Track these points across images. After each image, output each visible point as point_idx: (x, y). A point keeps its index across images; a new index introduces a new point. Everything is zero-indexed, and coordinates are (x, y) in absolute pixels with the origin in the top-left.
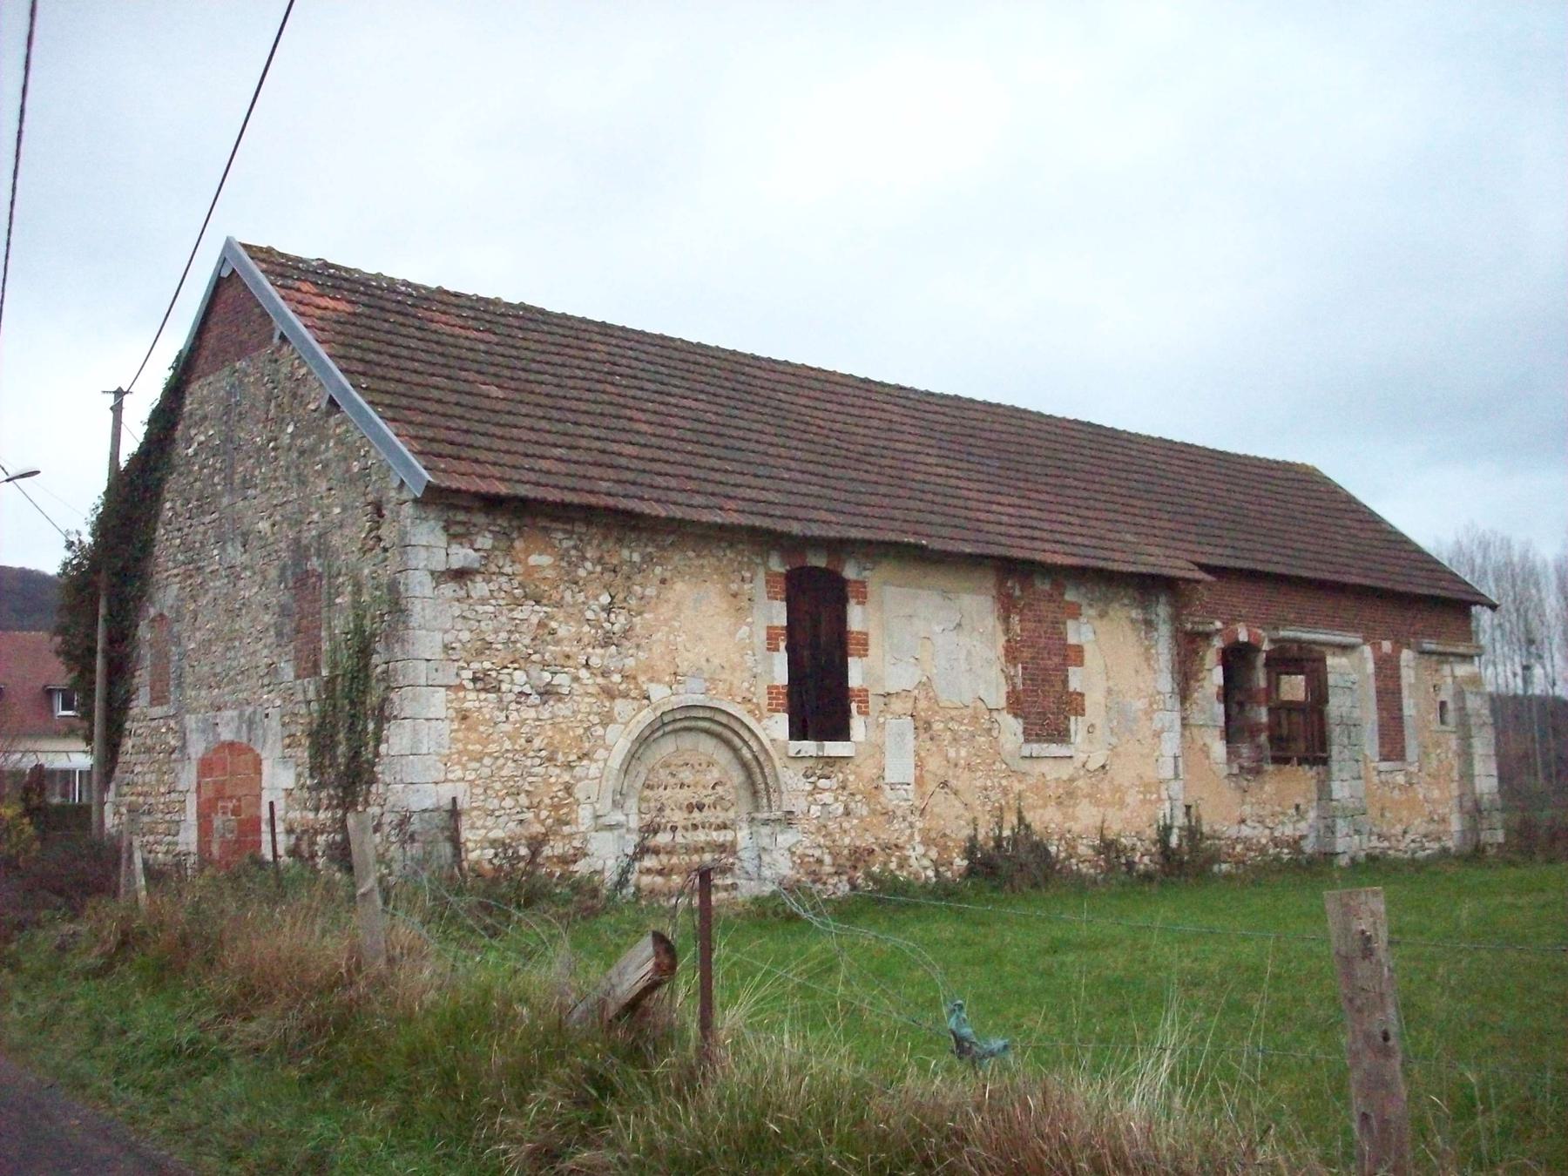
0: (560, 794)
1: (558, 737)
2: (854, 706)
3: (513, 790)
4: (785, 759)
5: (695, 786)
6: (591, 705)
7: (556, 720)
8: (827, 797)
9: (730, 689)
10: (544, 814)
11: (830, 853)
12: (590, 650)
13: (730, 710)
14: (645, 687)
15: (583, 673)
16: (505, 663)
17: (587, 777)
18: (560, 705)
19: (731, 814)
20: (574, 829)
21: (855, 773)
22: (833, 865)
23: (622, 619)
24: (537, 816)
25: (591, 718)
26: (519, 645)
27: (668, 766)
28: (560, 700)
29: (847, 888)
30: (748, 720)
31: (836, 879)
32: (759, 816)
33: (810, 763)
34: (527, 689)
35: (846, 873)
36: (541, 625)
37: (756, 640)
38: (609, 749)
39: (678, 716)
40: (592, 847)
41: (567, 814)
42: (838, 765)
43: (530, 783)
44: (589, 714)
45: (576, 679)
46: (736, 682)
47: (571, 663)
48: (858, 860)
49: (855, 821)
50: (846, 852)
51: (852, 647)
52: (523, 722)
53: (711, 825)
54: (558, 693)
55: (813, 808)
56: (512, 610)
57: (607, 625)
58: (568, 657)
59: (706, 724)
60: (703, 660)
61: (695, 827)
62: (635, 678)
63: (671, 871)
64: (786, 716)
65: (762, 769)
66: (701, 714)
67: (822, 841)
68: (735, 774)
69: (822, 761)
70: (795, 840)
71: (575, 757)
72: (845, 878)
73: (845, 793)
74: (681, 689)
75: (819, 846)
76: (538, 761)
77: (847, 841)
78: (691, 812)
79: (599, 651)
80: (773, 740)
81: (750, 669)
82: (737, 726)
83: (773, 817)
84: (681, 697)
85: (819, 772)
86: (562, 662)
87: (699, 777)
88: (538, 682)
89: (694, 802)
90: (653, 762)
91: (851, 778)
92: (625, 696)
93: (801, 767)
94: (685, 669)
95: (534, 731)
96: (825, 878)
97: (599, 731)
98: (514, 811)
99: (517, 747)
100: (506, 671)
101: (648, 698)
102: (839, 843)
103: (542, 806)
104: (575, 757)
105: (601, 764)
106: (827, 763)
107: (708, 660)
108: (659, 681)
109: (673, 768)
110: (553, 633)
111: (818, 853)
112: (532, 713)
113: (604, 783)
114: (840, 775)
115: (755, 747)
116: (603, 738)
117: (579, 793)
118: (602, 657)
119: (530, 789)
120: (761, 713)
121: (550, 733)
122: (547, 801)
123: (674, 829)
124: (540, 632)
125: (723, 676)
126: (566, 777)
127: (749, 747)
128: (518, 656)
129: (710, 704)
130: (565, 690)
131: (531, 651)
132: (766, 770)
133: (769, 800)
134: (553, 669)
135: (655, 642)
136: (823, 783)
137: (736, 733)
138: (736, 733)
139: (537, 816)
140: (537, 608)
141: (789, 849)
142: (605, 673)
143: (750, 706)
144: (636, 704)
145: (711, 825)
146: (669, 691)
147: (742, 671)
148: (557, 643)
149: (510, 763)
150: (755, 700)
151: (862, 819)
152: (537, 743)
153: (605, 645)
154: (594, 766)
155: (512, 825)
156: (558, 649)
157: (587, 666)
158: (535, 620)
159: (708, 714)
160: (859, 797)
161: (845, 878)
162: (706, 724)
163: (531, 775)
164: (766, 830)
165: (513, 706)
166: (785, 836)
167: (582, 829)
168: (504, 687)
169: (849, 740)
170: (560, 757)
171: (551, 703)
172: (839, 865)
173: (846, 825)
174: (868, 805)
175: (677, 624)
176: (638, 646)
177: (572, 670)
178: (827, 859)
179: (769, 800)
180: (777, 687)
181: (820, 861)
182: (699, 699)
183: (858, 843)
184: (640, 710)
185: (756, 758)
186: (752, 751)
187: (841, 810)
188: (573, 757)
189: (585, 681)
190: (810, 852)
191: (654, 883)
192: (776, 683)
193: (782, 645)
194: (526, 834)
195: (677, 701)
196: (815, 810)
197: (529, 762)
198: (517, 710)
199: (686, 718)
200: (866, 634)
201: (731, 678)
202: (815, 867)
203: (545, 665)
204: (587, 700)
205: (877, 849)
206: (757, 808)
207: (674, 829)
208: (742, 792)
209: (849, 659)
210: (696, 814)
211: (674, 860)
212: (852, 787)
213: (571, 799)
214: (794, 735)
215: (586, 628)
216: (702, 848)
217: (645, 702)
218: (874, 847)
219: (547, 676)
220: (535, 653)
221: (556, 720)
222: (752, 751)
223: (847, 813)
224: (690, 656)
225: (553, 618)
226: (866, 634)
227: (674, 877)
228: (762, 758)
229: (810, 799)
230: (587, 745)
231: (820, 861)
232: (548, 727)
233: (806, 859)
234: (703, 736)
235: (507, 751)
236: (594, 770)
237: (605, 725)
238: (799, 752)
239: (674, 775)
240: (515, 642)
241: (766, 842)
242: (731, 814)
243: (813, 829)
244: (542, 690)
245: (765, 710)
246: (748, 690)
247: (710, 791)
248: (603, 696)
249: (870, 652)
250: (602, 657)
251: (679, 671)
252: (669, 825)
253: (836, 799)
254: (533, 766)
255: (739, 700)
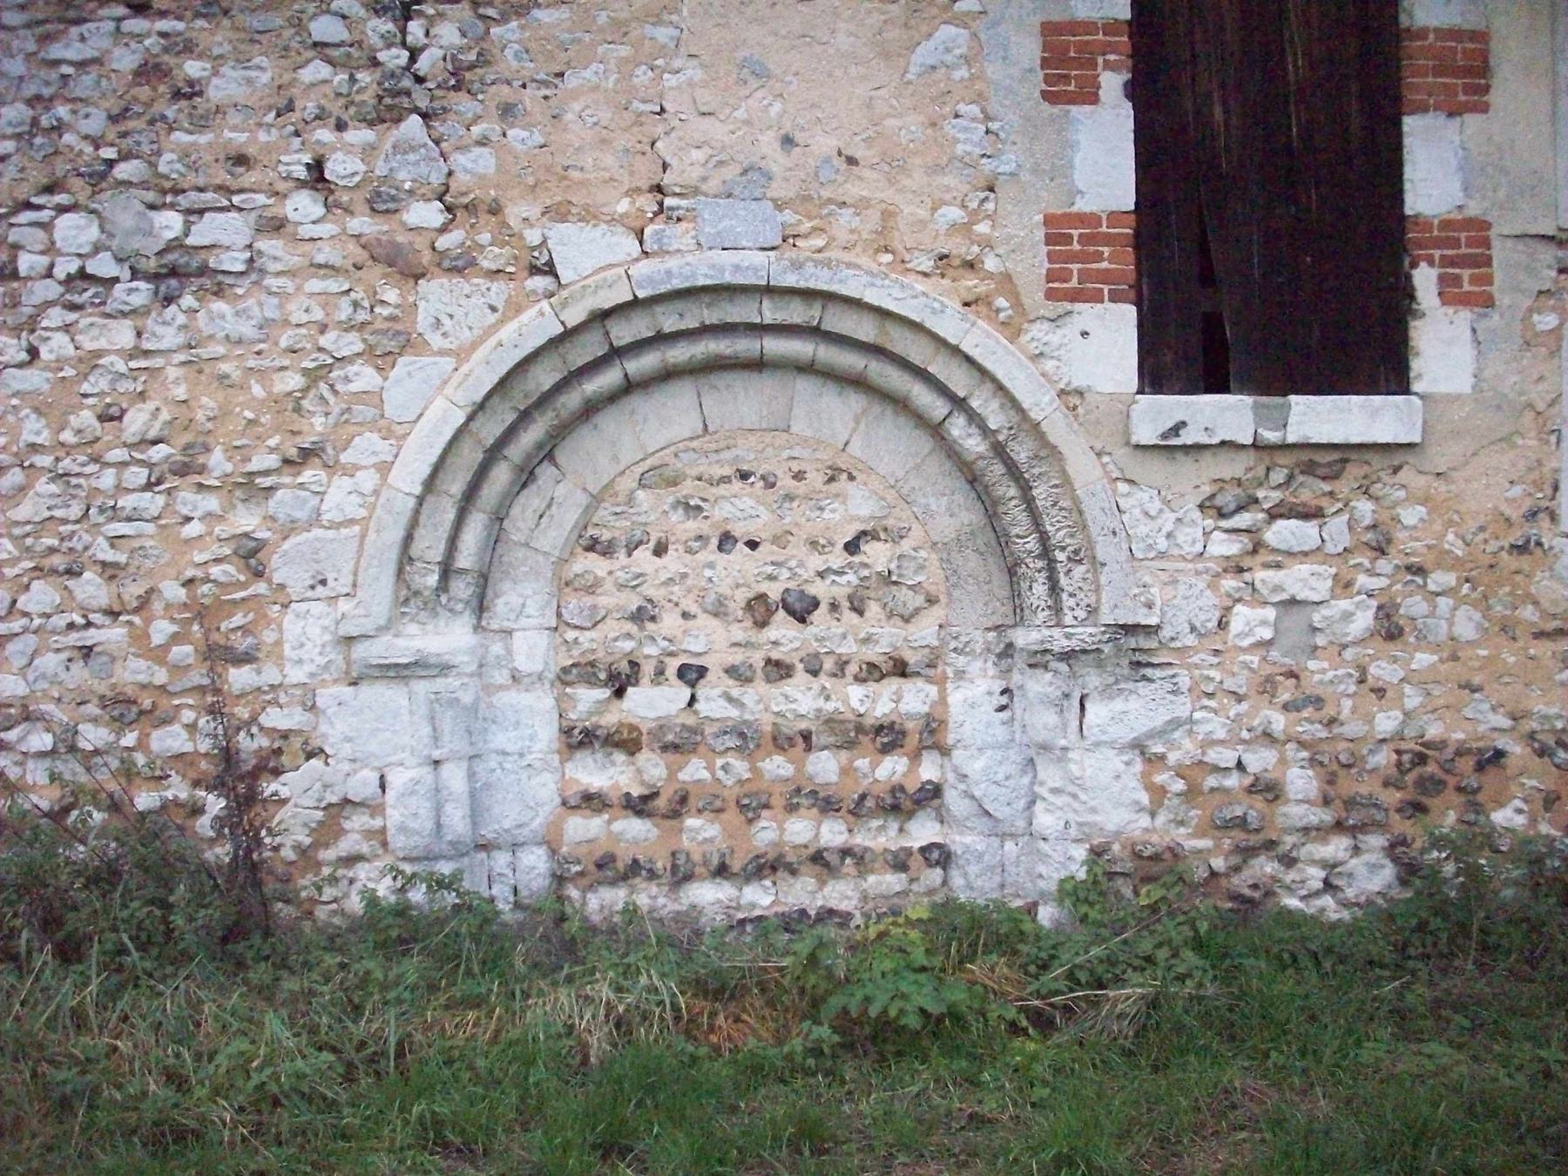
0: (216, 571)
1: (208, 402)
2: (1425, 279)
3: (58, 561)
4: (1121, 453)
5: (780, 540)
6: (326, 299)
7: (204, 352)
8: (1305, 580)
9: (883, 231)
10: (161, 630)
11: (1313, 762)
12: (325, 135)
13: (871, 297)
14: (533, 237)
15: (303, 206)
16: (22, 192)
17: (315, 520)
18: (219, 306)
19: (925, 631)
20: (270, 675)
21: (1425, 501)
22: (1326, 802)
23: (448, 34)
24: (139, 638)
25: (325, 341)
26: (68, 138)
27: (673, 482)
28: (219, 292)
29: (1388, 872)
30: (978, 338)
31: (1337, 847)
32: (1024, 638)
33: (1233, 467)
34: (103, 266)
35: (1381, 827)
36: (149, 71)
37: (993, 70)
38: (394, 433)
39: (670, 324)
40: (333, 731)
41: (244, 629)
42: (1354, 472)
43: (114, 541)
44: (323, 328)
45: (276, 226)
46: (911, 210)
47: (250, 178)
48: (1431, 786)
49: (1423, 659)
50: (1383, 758)
51: (1418, 80)
52: (90, 362)
53: (842, 664)
54: (204, 270)
55: (1242, 616)
56: (46, 39)
57: (395, 58)
58: (241, 160)
59: (800, 348)
60: (768, 143)
61: (779, 670)
62: (495, 210)
63: (681, 804)
64: (1129, 312)
65: (1026, 489)
66: (770, 313)
67: (1279, 722)
68: (937, 504)
69: (1284, 459)
70: (1160, 719)
71: (272, 461)
72: (1376, 841)
73: (1384, 565)
74: (679, 237)
75: (1268, 737)
76: (138, 475)
77: (1386, 723)
78: (762, 624)
79: (359, 135)
80: (1070, 396)
81: (967, 163)
82: (917, 351)
83: (1060, 643)
84: (673, 263)
85: (1269, 497)
86: (222, 177)
87: (795, 514)
88: (136, 243)
89: (774, 592)
90: (607, 470)
91: (1411, 515)
92: (460, 266)
93: (1195, 479)
94: (695, 174)
95: (126, 386)
96: (1289, 840)
97: (364, 377)
98: (60, 621)
99: (67, 436)
100: (26, 216)
101: (550, 269)
102: (1353, 728)
103: (157, 606)
104: (272, 461)
105: (367, 480)
106: (1310, 469)
107: (788, 141)
108: (590, 216)
109: (687, 488)
110: (190, 92)
111: (1260, 760)
112: (122, 334)
113: (372, 536)
114: (1364, 508)
115: (996, 418)
116: (375, 398)
117: (286, 568)
118: (368, 151)
119: (109, 556)
120: (1017, 303)
121: (181, 392)
122: (174, 592)
123: (692, 674)
124: (144, 92)
125: (853, 191)
126: (246, 520)
127: (974, 418)
128: (61, 167)
129: (791, 280)
130: (233, 261)
131: (109, 153)
132: (1040, 492)
133: (1054, 588)
134: (192, 199)
135: (575, 94)
136: (1284, 533)
137: (922, 374)
138: (922, 374)
139: (139, 638)
140: (136, 25)
141: (1139, 746)
142: (383, 201)
143: (970, 282)
144: (499, 291)
145: (842, 664)
146: (633, 247)
147: (937, 169)
148: (201, 123)
149: (44, 486)
150: (991, 264)
151: (1453, 651)
152: (136, 421)
153: (386, 113)
154: (341, 484)
155: (50, 662)
156: (203, 139)
157: (317, 177)
158: (125, 60)
159: (796, 313)
160: (1440, 579)
161: (1376, 841)
162: (800, 348)
163: (114, 513)
164: (1039, 685)
165: (56, 317)
166: (1118, 705)
167: (296, 675)
168: (25, 263)
169: (1403, 387)
170: (218, 462)
171: (188, 301)
172: (1350, 803)
173: (1383, 671)
174: (1483, 604)
175: (663, 34)
176: (507, 111)
177: (261, 199)
178: (1300, 781)
179: (1054, 588)
180: (1083, 219)
181: (1269, 790)
182: (752, 265)
183: (1434, 731)
184: (514, 308)
185: (999, 450)
186: (985, 431)
187: (1364, 620)
188: (262, 461)
189: (307, 231)
190: (1226, 757)
191: (616, 838)
192: (1082, 206)
193: (1112, 83)
194: (103, 688)
195: (651, 276)
196: (1251, 622)
197: (108, 479)
198: (67, 328)
199: (706, 330)
200: (1480, 36)
201: (889, 194)
202: (1253, 809)
203: (165, 193)
204: (315, 285)
205: (1516, 750)
206: (1020, 613)
207: (692, 674)
208: (970, 562)
209: (1409, 123)
210: (782, 629)
211: (695, 770)
212: (1410, 545)
213: (261, 588)
214: (1154, 377)
215: (317, 70)
216: (806, 736)
217: (540, 283)
218: (1501, 742)
219: (169, 223)
220: (125, 156)
221: (204, 352)
222: (985, 431)
223: (1390, 629)
224: (716, 130)
225: (188, 48)
226: (1480, 36)
227: (691, 822)
228: (1021, 452)
229: (1230, 583)
230: (319, 423)
231: (1269, 790)
232: (172, 373)
233: (1211, 781)
234: (804, 386)
235: (34, 448)
236: (340, 497)
237: (382, 360)
238: (1176, 429)
239: (693, 510)
240: (59, 128)
241: (1043, 722)
242: (925, 631)
243: (1239, 683)
244: (151, 265)
245: (1033, 296)
246: (964, 229)
247: (837, 559)
248: (374, 273)
249: (1495, 97)
250: (368, 151)
251: (667, 180)
252: (673, 665)
253: (1343, 586)
254: (120, 489)
255: (926, 264)
